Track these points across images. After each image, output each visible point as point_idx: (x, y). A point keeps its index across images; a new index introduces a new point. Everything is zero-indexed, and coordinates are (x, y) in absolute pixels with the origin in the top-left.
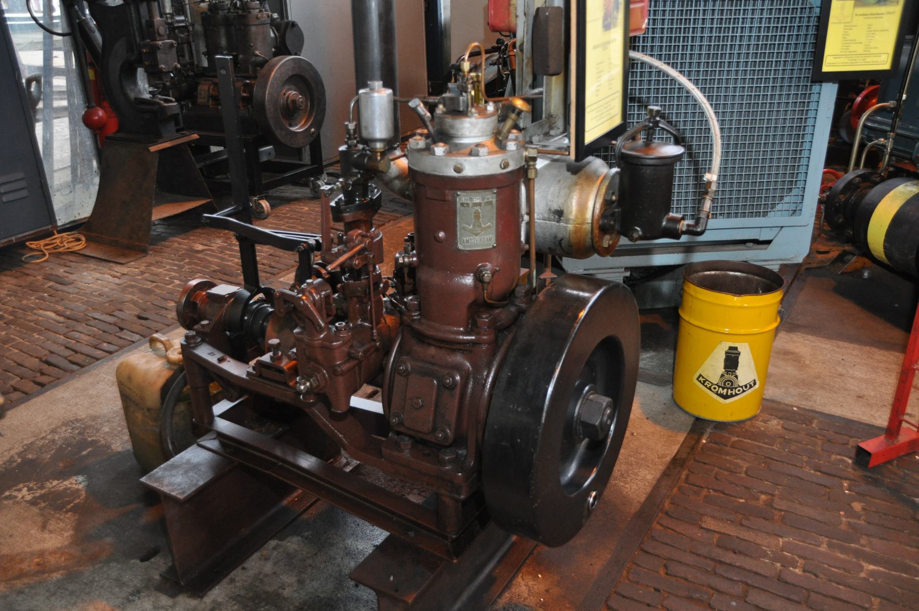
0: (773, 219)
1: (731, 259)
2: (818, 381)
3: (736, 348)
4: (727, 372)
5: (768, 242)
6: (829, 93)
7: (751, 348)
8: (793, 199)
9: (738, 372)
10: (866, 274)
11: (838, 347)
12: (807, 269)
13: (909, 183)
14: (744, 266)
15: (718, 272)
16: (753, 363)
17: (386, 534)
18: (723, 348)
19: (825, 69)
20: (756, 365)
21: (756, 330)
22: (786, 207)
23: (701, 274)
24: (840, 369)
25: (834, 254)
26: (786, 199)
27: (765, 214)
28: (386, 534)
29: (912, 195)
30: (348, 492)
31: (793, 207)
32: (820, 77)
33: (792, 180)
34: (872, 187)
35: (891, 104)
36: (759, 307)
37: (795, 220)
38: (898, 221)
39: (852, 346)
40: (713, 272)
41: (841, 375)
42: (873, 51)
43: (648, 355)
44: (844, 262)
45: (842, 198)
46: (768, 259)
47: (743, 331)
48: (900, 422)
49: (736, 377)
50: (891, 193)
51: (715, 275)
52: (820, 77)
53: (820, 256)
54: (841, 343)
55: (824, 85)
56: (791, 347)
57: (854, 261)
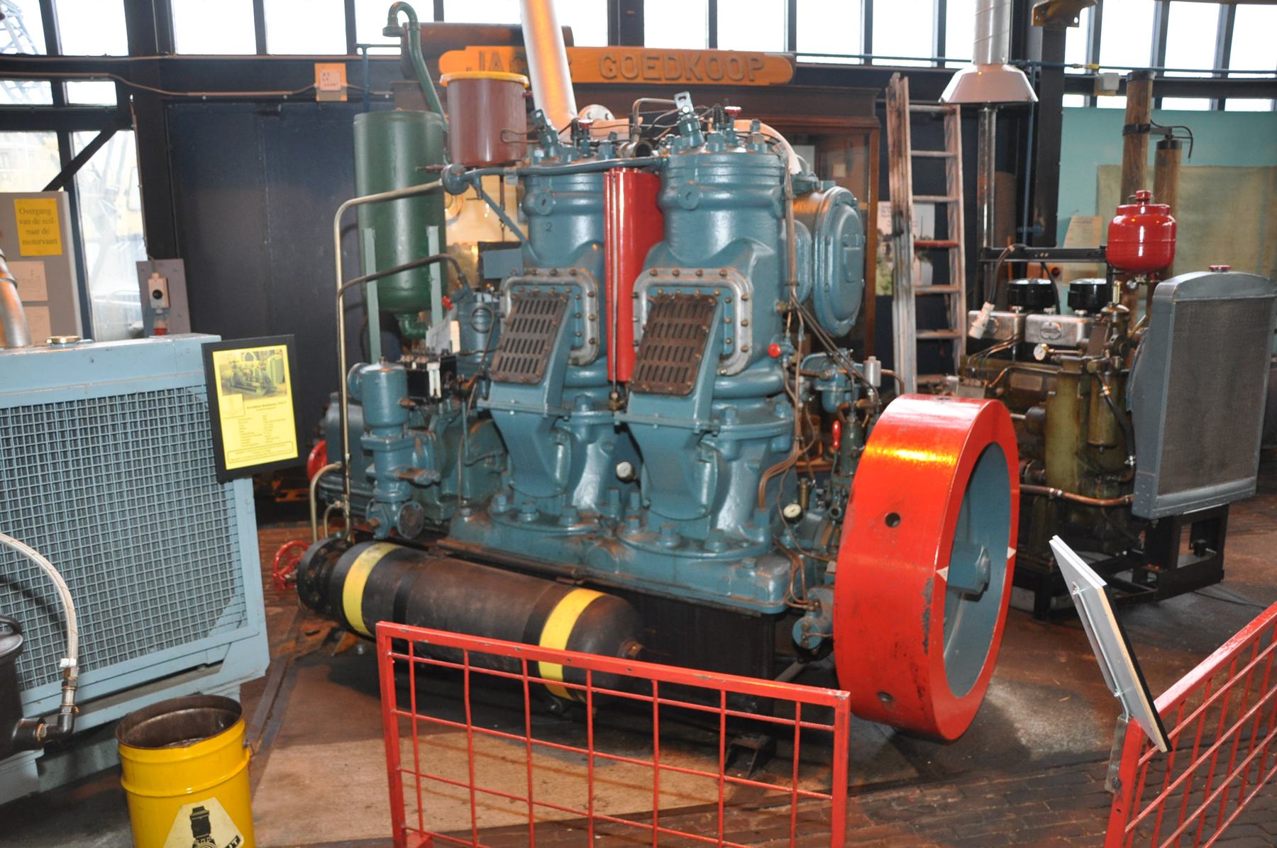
0: (218, 636)
1: (173, 697)
2: (321, 803)
3: (202, 808)
4: (199, 840)
5: (221, 662)
6: (243, 492)
7: (222, 803)
8: (235, 609)
9: (212, 835)
10: (361, 650)
11: (339, 751)
12: (298, 659)
13: (371, 548)
14: (197, 700)
15: (165, 716)
16: (228, 818)
17: (1179, 566)
18: (187, 810)
19: (229, 466)
20: (233, 819)
21: (223, 778)
22: (229, 619)
23: (143, 724)
24: (344, 779)
25: (324, 633)
26: (226, 611)
27: (205, 634)
28: (1179, 566)
29: (376, 561)
30: (1033, 172)
31: (237, 618)
32: (225, 476)
33: (227, 588)
34: (339, 556)
35: (336, 465)
36: (216, 752)
37: (242, 632)
38: (370, 591)
39: (354, 744)
40: (159, 718)
41: (346, 786)
42: (275, 441)
43: (105, 840)
44: (336, 641)
45: (312, 574)
46: (225, 684)
47: (207, 785)
48: (404, 831)
49: (212, 841)
50: (356, 563)
51: (162, 720)
52: (225, 476)
53: (310, 639)
54: (342, 745)
55: (235, 482)
56: (287, 768)
57: (344, 636)
